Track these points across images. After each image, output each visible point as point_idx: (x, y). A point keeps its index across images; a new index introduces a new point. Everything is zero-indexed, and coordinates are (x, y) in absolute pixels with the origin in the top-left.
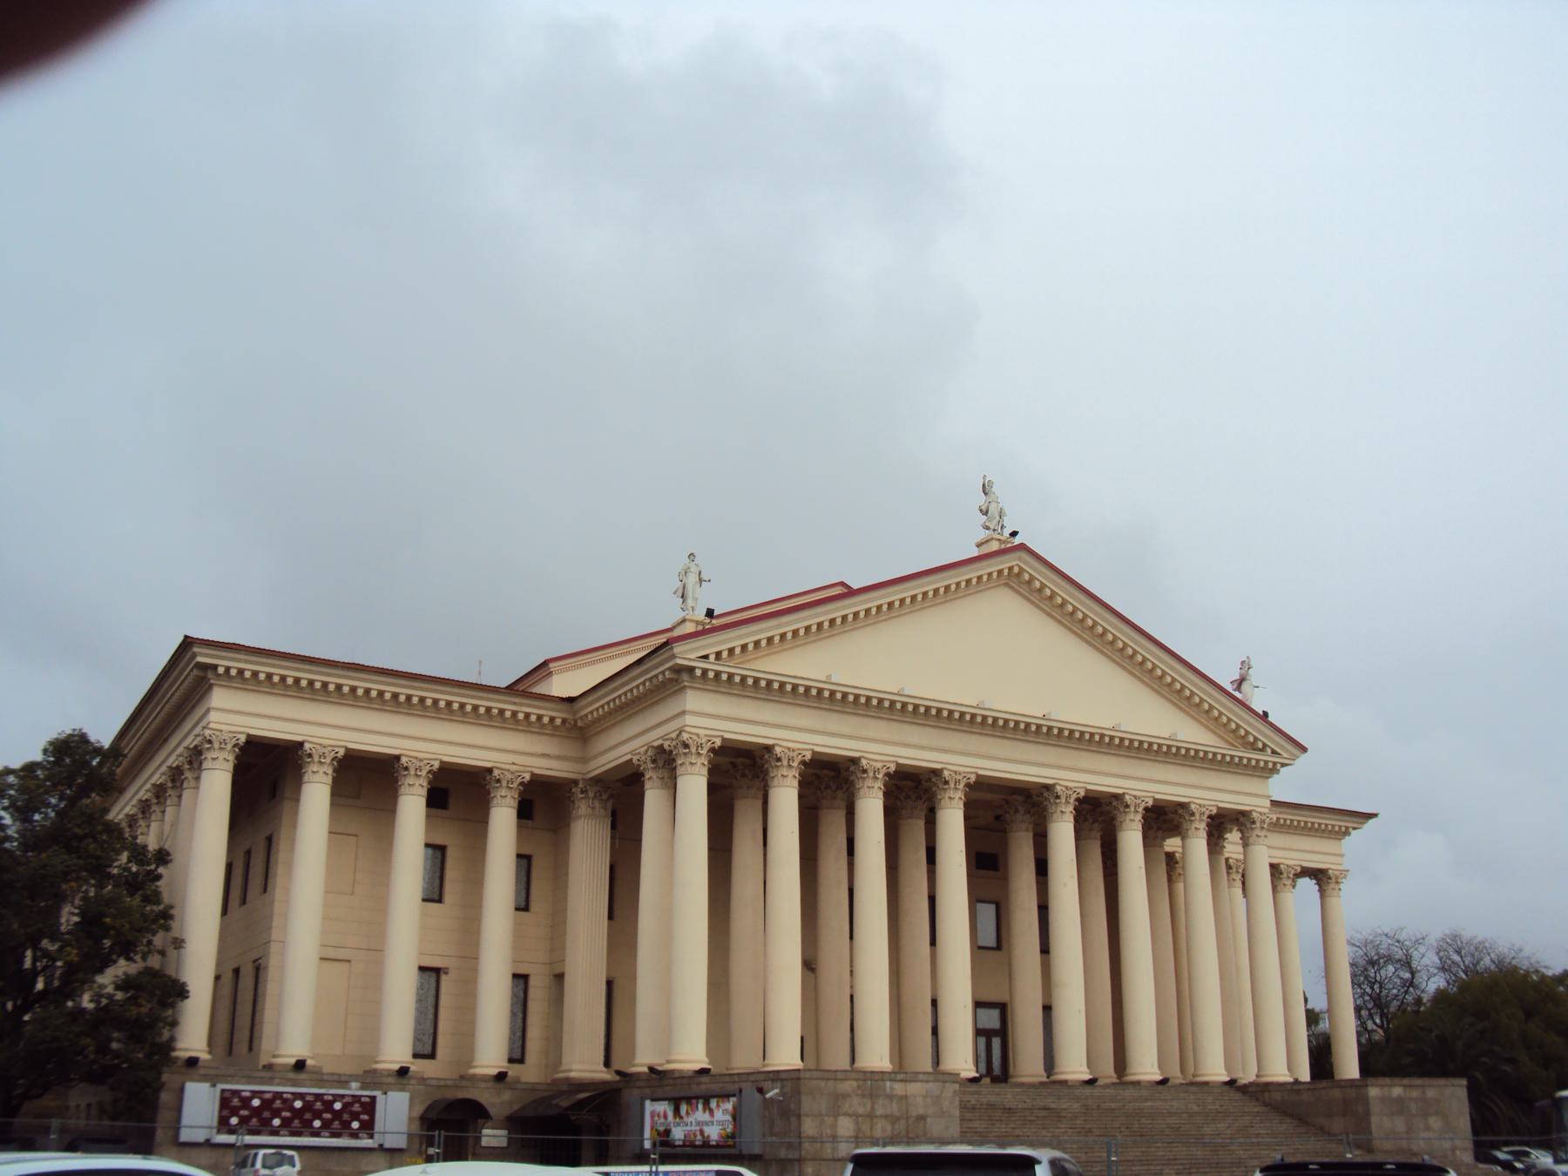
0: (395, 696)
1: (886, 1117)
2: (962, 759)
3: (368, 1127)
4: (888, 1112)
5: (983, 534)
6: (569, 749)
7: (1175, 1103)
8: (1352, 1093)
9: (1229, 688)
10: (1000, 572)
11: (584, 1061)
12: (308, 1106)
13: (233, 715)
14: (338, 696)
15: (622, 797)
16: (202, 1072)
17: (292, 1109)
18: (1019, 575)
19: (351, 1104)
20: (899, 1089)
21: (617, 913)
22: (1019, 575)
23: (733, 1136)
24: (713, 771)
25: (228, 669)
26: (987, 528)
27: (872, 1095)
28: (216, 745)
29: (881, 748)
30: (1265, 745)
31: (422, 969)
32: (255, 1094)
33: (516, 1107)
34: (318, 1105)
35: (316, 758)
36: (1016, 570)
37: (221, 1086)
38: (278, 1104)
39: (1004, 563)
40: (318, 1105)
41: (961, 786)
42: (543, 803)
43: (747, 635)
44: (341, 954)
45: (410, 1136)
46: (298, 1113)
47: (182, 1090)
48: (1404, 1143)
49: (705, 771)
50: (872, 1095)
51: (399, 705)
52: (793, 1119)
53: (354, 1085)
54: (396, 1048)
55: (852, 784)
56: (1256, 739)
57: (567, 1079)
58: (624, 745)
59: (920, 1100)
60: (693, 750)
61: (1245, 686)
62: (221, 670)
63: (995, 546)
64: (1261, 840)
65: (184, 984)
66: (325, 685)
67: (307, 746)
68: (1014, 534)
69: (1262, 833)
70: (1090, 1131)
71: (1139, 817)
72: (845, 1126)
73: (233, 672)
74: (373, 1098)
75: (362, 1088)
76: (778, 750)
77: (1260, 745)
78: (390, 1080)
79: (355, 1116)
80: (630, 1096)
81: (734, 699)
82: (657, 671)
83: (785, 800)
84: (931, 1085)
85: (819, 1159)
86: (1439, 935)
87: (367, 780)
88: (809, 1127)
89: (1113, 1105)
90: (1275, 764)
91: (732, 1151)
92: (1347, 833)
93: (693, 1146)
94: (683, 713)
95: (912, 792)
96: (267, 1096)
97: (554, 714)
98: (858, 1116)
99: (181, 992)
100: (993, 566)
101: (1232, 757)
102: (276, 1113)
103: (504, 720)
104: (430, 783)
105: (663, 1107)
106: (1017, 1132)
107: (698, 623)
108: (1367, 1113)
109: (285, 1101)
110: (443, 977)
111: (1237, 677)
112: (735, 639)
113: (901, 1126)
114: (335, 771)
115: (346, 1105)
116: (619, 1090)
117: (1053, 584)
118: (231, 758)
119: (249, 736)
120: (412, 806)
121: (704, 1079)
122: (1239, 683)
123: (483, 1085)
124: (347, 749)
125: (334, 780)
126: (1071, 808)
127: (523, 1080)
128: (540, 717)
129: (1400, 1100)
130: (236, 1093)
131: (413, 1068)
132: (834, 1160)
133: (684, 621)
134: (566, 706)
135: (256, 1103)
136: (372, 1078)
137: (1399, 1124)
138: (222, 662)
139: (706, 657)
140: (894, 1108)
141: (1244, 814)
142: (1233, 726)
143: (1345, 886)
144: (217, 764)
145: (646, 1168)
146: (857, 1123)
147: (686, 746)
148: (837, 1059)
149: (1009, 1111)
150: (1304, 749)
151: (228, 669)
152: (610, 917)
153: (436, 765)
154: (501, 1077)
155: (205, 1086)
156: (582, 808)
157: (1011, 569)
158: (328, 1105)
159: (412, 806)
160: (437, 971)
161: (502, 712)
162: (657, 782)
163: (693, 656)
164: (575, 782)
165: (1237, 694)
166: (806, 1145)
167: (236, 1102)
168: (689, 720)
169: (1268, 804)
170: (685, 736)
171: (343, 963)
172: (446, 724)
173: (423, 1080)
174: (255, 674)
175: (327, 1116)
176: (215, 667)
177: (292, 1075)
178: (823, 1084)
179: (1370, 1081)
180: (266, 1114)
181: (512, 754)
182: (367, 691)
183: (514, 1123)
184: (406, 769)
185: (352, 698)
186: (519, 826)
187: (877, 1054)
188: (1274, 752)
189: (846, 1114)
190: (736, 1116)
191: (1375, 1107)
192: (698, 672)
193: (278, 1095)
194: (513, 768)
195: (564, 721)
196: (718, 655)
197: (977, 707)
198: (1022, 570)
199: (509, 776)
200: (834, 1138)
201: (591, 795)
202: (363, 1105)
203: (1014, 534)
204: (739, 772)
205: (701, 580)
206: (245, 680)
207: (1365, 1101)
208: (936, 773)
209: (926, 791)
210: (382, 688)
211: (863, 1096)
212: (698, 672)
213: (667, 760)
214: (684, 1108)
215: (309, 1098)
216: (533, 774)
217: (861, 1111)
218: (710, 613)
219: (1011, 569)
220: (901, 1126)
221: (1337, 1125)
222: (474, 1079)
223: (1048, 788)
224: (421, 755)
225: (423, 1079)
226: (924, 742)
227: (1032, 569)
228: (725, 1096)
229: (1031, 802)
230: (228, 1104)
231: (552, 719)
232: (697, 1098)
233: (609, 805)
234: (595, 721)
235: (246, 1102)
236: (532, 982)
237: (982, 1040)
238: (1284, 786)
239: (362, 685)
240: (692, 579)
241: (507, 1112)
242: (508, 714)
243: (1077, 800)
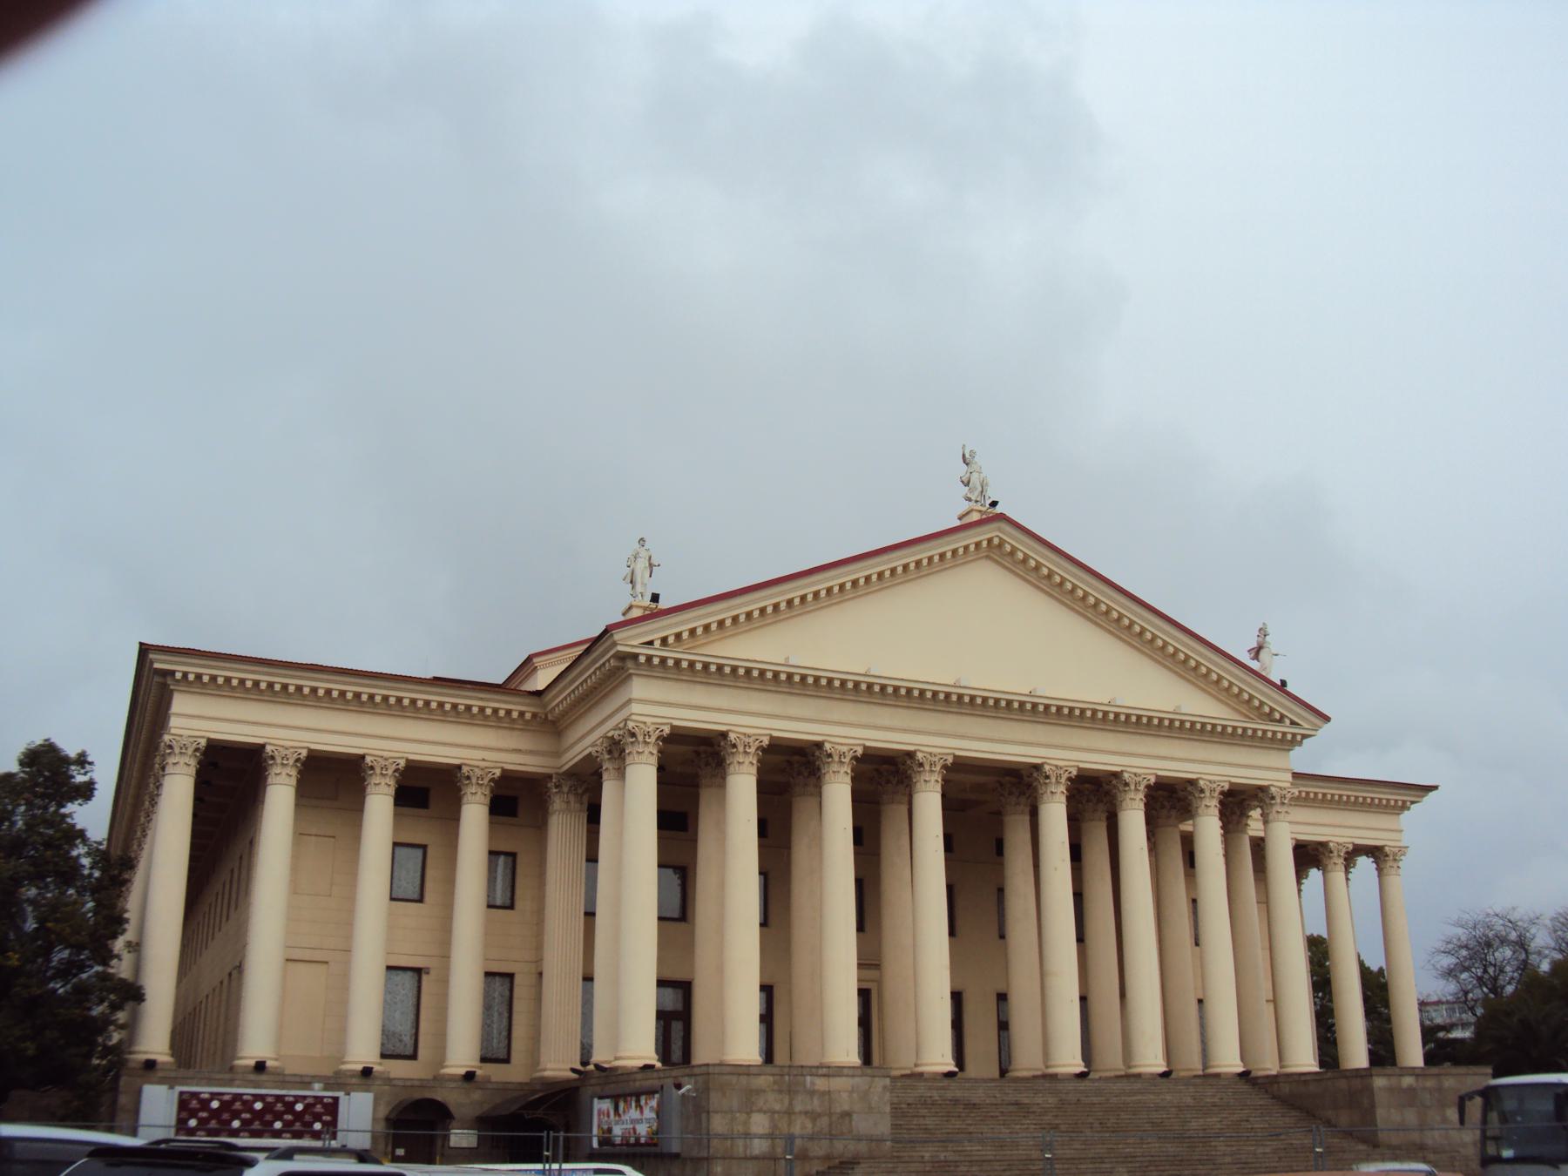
0: (357, 695)
1: (806, 1113)
2: (936, 740)
3: (332, 1128)
4: (809, 1108)
5: (966, 506)
6: (543, 743)
7: (1168, 1097)
8: (1357, 1083)
9: (1246, 659)
10: (978, 545)
11: (558, 1063)
12: (269, 1107)
13: (196, 720)
14: (299, 697)
16: (160, 1074)
18: (1000, 545)
19: (314, 1105)
21: (772, 920)
22: (1000, 545)
23: (656, 1133)
24: (856, 780)
25: (185, 675)
26: (969, 500)
27: (791, 1091)
28: (177, 750)
29: (846, 731)
30: (1282, 716)
31: (488, 974)
32: (214, 1096)
33: (486, 1107)
34: (279, 1106)
35: (378, 771)
36: (996, 541)
37: (179, 1089)
38: (238, 1105)
39: (983, 534)
40: (279, 1106)
41: (938, 768)
42: (515, 800)
43: (696, 619)
44: (318, 956)
45: (374, 1139)
46: (258, 1115)
47: (139, 1093)
48: (1415, 1137)
49: (848, 779)
50: (791, 1091)
51: (361, 704)
52: (704, 1116)
53: (317, 1086)
54: (363, 1049)
55: (1035, 790)
56: (1272, 710)
57: (542, 1078)
58: (585, 739)
59: (845, 1095)
60: (640, 738)
61: (1263, 654)
62: (178, 676)
63: (975, 517)
64: (1281, 816)
65: (140, 988)
66: (285, 687)
67: (269, 749)
68: (994, 504)
69: (1284, 809)
70: (1056, 1127)
71: (1141, 795)
72: (759, 1123)
73: (191, 677)
74: (336, 1099)
75: (325, 1089)
76: (920, 756)
77: (1277, 716)
78: (354, 1081)
79: (318, 1118)
80: (586, 1092)
81: (684, 685)
82: (601, 664)
83: (838, 796)
84: (857, 1080)
85: (728, 1157)
86: (1552, 914)
87: (332, 781)
88: (718, 1124)
89: (1095, 1100)
90: (1294, 735)
91: (653, 1149)
92: (1404, 807)
93: (628, 1144)
94: (630, 701)
95: (881, 778)
96: (226, 1098)
97: (523, 708)
98: (774, 1112)
99: (132, 993)
100: (970, 538)
101: (1245, 729)
102: (236, 1115)
103: (445, 713)
104: (397, 782)
105: (606, 1105)
106: (971, 1129)
107: (645, 608)
108: (1373, 1106)
109: (245, 1103)
110: (425, 977)
111: (1255, 645)
112: (681, 623)
113: (824, 1121)
114: (300, 772)
115: (307, 1107)
116: (577, 1088)
117: (1037, 555)
118: (193, 762)
119: (209, 740)
120: (379, 805)
121: (649, 1073)
122: (1257, 652)
123: (453, 1085)
124: (310, 751)
125: (299, 781)
126: (1062, 788)
127: (494, 1079)
128: (509, 712)
129: (1411, 1089)
130: (195, 1095)
131: (479, 1072)
132: (746, 1158)
133: (630, 607)
134: (535, 700)
135: (215, 1104)
136: (339, 1081)
137: (1411, 1116)
138: (179, 667)
139: (651, 643)
141: (1263, 789)
142: (1256, 703)
143: (1405, 862)
144: (177, 769)
145: (539, 1166)
146: (772, 1120)
147: (633, 735)
148: (1110, 1060)
149: (972, 1106)
150: (1327, 719)
151: (185, 675)
152: (952, 933)
153: (402, 763)
154: (469, 1076)
155: (161, 1090)
156: (557, 803)
157: (990, 541)
158: (289, 1107)
159: (379, 805)
160: (418, 971)
161: (468, 708)
162: (613, 773)
163: (635, 643)
164: (550, 777)
165: (1254, 665)
166: (715, 1143)
167: (194, 1104)
168: (635, 708)
169: (1289, 777)
170: (631, 725)
171: (326, 967)
172: (299, 709)
173: (388, 1081)
174: (228, 680)
175: (289, 1117)
176: (173, 673)
177: (253, 1077)
178: (734, 1079)
179: (1375, 1070)
180: (226, 1116)
181: (481, 750)
182: (372, 697)
183: (483, 1122)
184: (372, 768)
185: (314, 699)
186: (297, 805)
187: (1069, 1059)
188: (1293, 723)
189: (760, 1111)
190: (659, 1112)
191: (1381, 1098)
192: (642, 659)
193: (237, 1097)
194: (483, 764)
195: (534, 715)
196: (664, 641)
197: (1109, 704)
199: (478, 772)
200: (747, 1136)
201: (565, 789)
202: (325, 1105)
203: (994, 504)
204: (691, 765)
205: (651, 566)
206: (418, 710)
207: (1369, 1090)
208: (1116, 775)
209: (1179, 800)
210: (496, 705)
211: (780, 1091)
212: (642, 659)
213: (617, 749)
214: (622, 1105)
215: (269, 1100)
216: (504, 770)
217: (777, 1107)
218: (655, 598)
219: (990, 541)
220: (824, 1121)
221: (1344, 1119)
222: (439, 1079)
223: (1116, 775)
224: (385, 754)
225: (390, 1080)
226: (768, 709)
227: (1012, 539)
228: (651, 1093)
229: (1020, 783)
230: (186, 1106)
231: (522, 714)
232: (631, 1095)
233: (585, 799)
234: (565, 713)
235: (205, 1104)
236: (517, 980)
238: (1303, 759)
239: (307, 684)
240: (641, 565)
241: (478, 1113)
242: (475, 710)
243: (1148, 787)
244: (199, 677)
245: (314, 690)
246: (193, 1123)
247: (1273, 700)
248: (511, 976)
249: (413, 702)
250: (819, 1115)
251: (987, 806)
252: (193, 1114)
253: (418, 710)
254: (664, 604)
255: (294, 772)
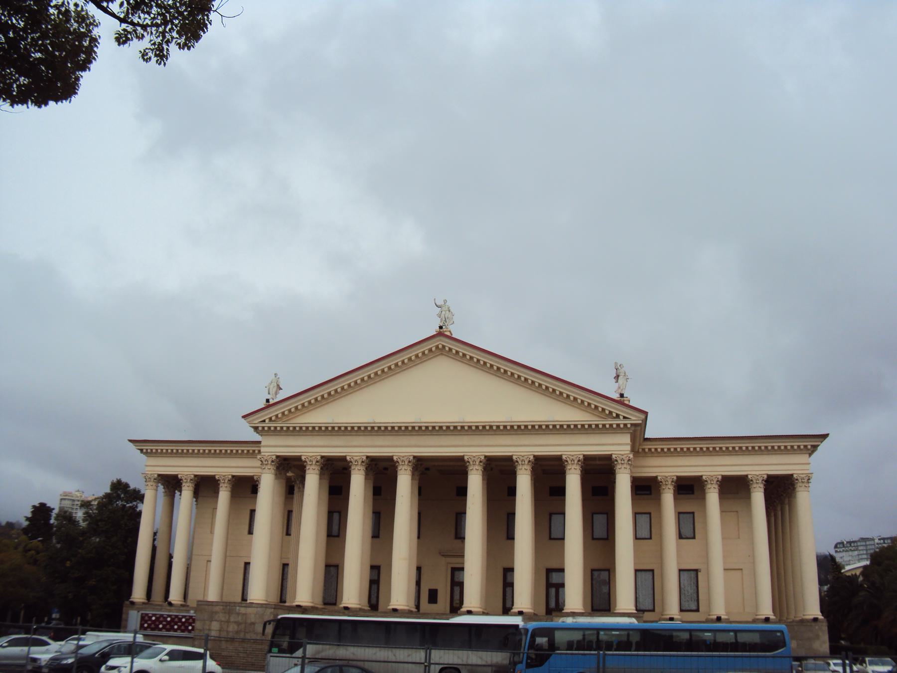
1: (235, 622)
12: (172, 620)
14: (714, 452)
15: (245, 487)
17: (166, 621)
20: (243, 610)
27: (230, 613)
30: (618, 416)
32: (154, 615)
36: (440, 346)
50: (230, 613)
53: (192, 612)
59: (253, 616)
72: (215, 626)
77: (614, 415)
102: (161, 623)
110: (699, 574)
113: (243, 626)
114: (719, 486)
115: (187, 620)
130: (147, 615)
135: (169, 619)
139: (264, 421)
140: (240, 619)
152: (419, 537)
155: (136, 612)
158: (180, 620)
167: (146, 618)
188: (624, 417)
193: (162, 616)
196: (270, 419)
198: (444, 347)
217: (223, 619)
220: (243, 626)
235: (165, 619)
237: (553, 591)
244: (779, 447)
245: (669, 449)
246: (146, 625)
247: (616, 409)
248: (652, 571)
249: (792, 447)
250: (241, 623)
251: (441, 482)
252: (146, 622)
253: (782, 450)
254: (271, 402)
255: (716, 486)
